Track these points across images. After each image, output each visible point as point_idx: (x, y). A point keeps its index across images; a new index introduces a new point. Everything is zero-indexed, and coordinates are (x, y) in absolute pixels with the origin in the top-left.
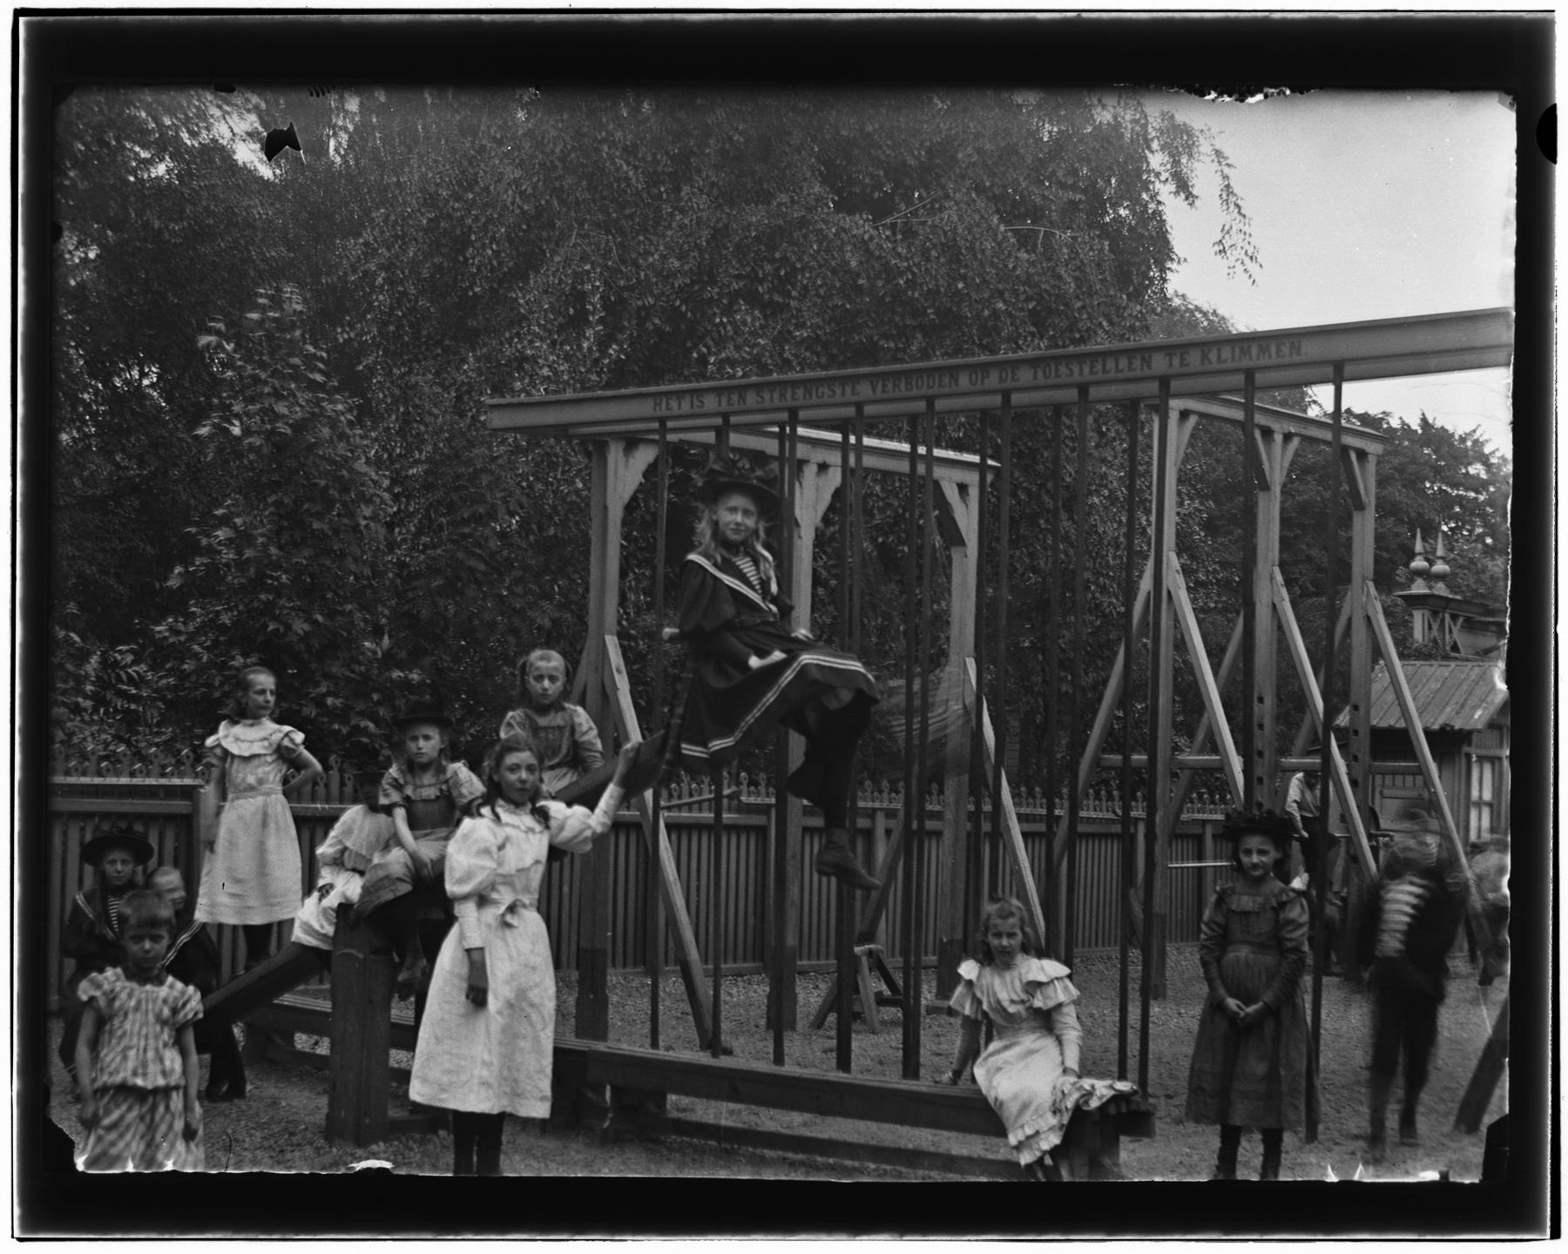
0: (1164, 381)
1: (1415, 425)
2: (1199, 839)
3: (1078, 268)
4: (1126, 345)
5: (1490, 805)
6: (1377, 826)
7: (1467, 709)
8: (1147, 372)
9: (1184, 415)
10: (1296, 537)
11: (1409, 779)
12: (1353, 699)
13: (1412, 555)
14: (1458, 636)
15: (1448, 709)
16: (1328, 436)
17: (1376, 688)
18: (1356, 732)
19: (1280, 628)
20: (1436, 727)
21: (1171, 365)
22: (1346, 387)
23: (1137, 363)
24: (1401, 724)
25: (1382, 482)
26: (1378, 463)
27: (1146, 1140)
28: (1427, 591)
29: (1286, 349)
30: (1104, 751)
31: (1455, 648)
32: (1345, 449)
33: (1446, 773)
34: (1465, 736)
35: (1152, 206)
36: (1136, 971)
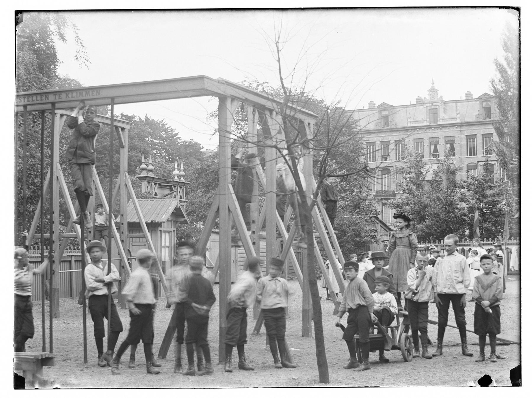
0: (53, 104)
1: (143, 119)
2: (70, 262)
3: (25, 65)
4: (42, 91)
5: (169, 247)
6: (131, 256)
7: (160, 215)
8: (48, 101)
9: (62, 115)
10: (102, 158)
11: (141, 239)
12: (121, 213)
13: (141, 163)
14: (157, 190)
15: (154, 215)
16: (109, 122)
17: (129, 209)
18: (122, 224)
19: (60, 188)
20: (150, 221)
21: (55, 98)
22: (115, 106)
23: (44, 98)
24: (138, 221)
25: (131, 138)
26: (129, 131)
27: (52, 367)
28: (146, 175)
29: (95, 93)
30: (36, 232)
31: (156, 194)
32: (117, 127)
33: (153, 236)
34: (159, 224)
35: (51, 44)
36: (47, 308)
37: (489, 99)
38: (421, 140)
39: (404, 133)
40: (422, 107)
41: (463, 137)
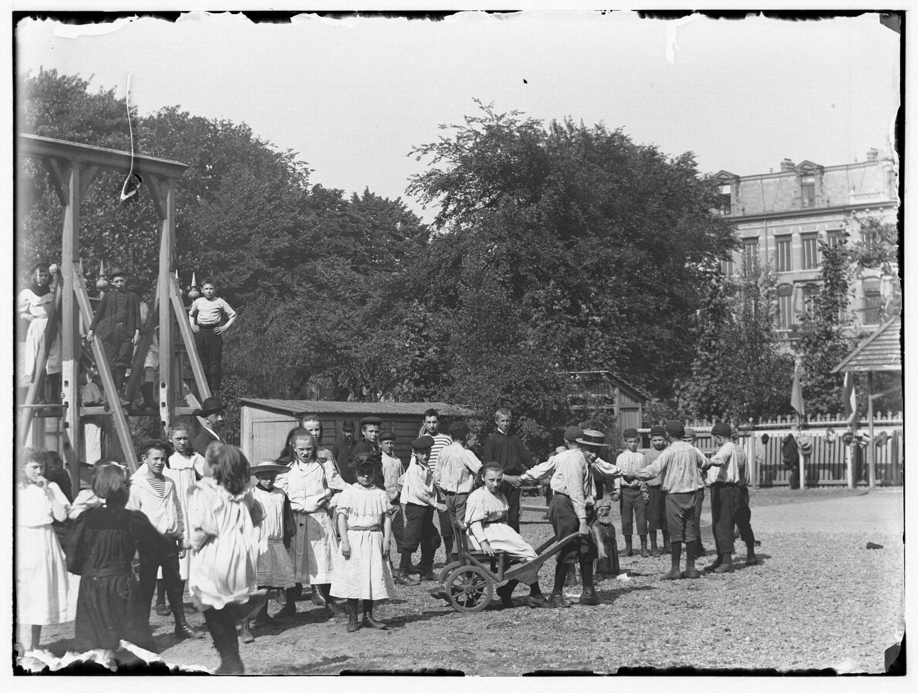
37: (810, 172)
38: (788, 239)
39: (842, 217)
40: (875, 167)
41: (771, 238)
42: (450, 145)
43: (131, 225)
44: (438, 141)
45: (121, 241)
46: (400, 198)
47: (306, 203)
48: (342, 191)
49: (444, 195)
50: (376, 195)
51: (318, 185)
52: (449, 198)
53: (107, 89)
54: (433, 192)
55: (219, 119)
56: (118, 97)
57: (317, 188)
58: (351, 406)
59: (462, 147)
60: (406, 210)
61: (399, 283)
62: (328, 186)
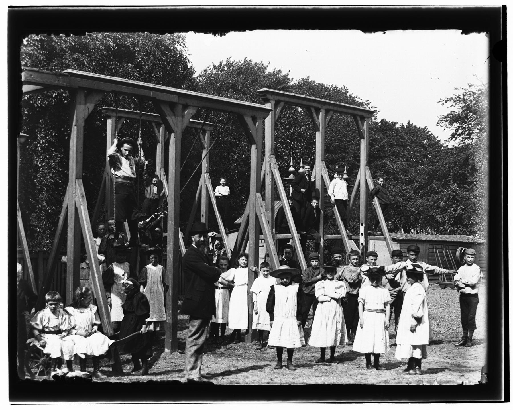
42: (460, 98)
43: (292, 140)
44: (454, 97)
45: (286, 148)
46: (426, 126)
47: (377, 129)
48: (396, 123)
49: (456, 125)
50: (414, 125)
51: (383, 119)
52: (459, 127)
53: (277, 69)
54: (451, 123)
55: (331, 85)
56: (284, 73)
57: (383, 121)
58: (414, 235)
59: (225, 80)
60: (430, 133)
61: (433, 172)
62: (389, 120)
